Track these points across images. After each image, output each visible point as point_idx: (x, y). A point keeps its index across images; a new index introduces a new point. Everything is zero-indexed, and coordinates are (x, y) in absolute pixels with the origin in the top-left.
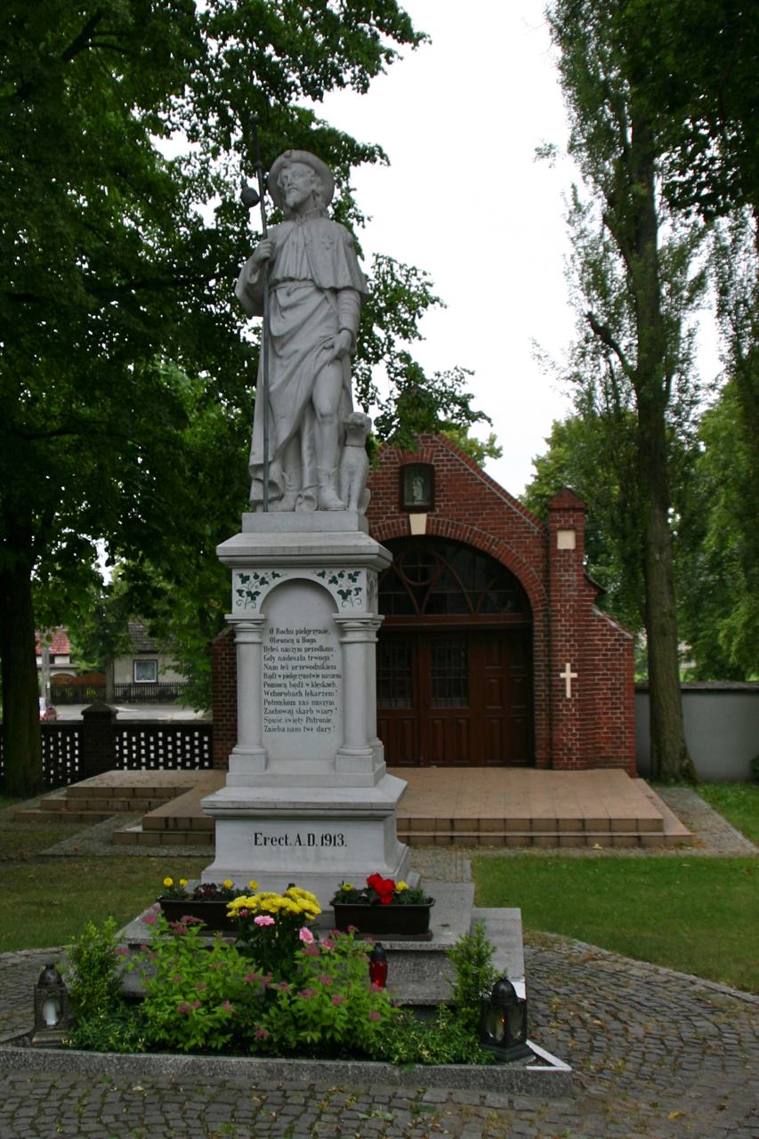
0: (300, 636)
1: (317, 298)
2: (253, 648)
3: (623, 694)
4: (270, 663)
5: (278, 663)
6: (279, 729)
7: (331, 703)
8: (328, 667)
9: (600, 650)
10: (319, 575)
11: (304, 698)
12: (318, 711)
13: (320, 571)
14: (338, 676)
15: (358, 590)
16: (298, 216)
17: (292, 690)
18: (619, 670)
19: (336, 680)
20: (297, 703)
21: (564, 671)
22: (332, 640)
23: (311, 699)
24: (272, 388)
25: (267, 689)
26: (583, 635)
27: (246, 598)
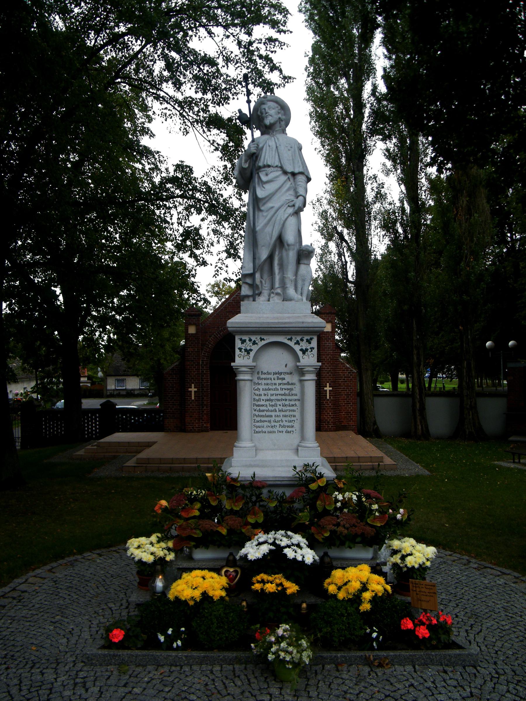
0: (275, 376)
1: (283, 178)
2: (248, 383)
3: (352, 397)
4: (257, 392)
5: (262, 392)
6: (263, 432)
7: (294, 416)
8: (292, 395)
9: (342, 377)
10: (288, 339)
11: (278, 413)
12: (286, 421)
13: (289, 337)
14: (299, 400)
15: (312, 348)
16: (271, 131)
17: (271, 408)
18: (350, 386)
19: (297, 403)
20: (274, 416)
21: (326, 387)
22: (295, 379)
23: (282, 414)
24: (258, 229)
25: (255, 407)
26: (335, 371)
27: (244, 353)
